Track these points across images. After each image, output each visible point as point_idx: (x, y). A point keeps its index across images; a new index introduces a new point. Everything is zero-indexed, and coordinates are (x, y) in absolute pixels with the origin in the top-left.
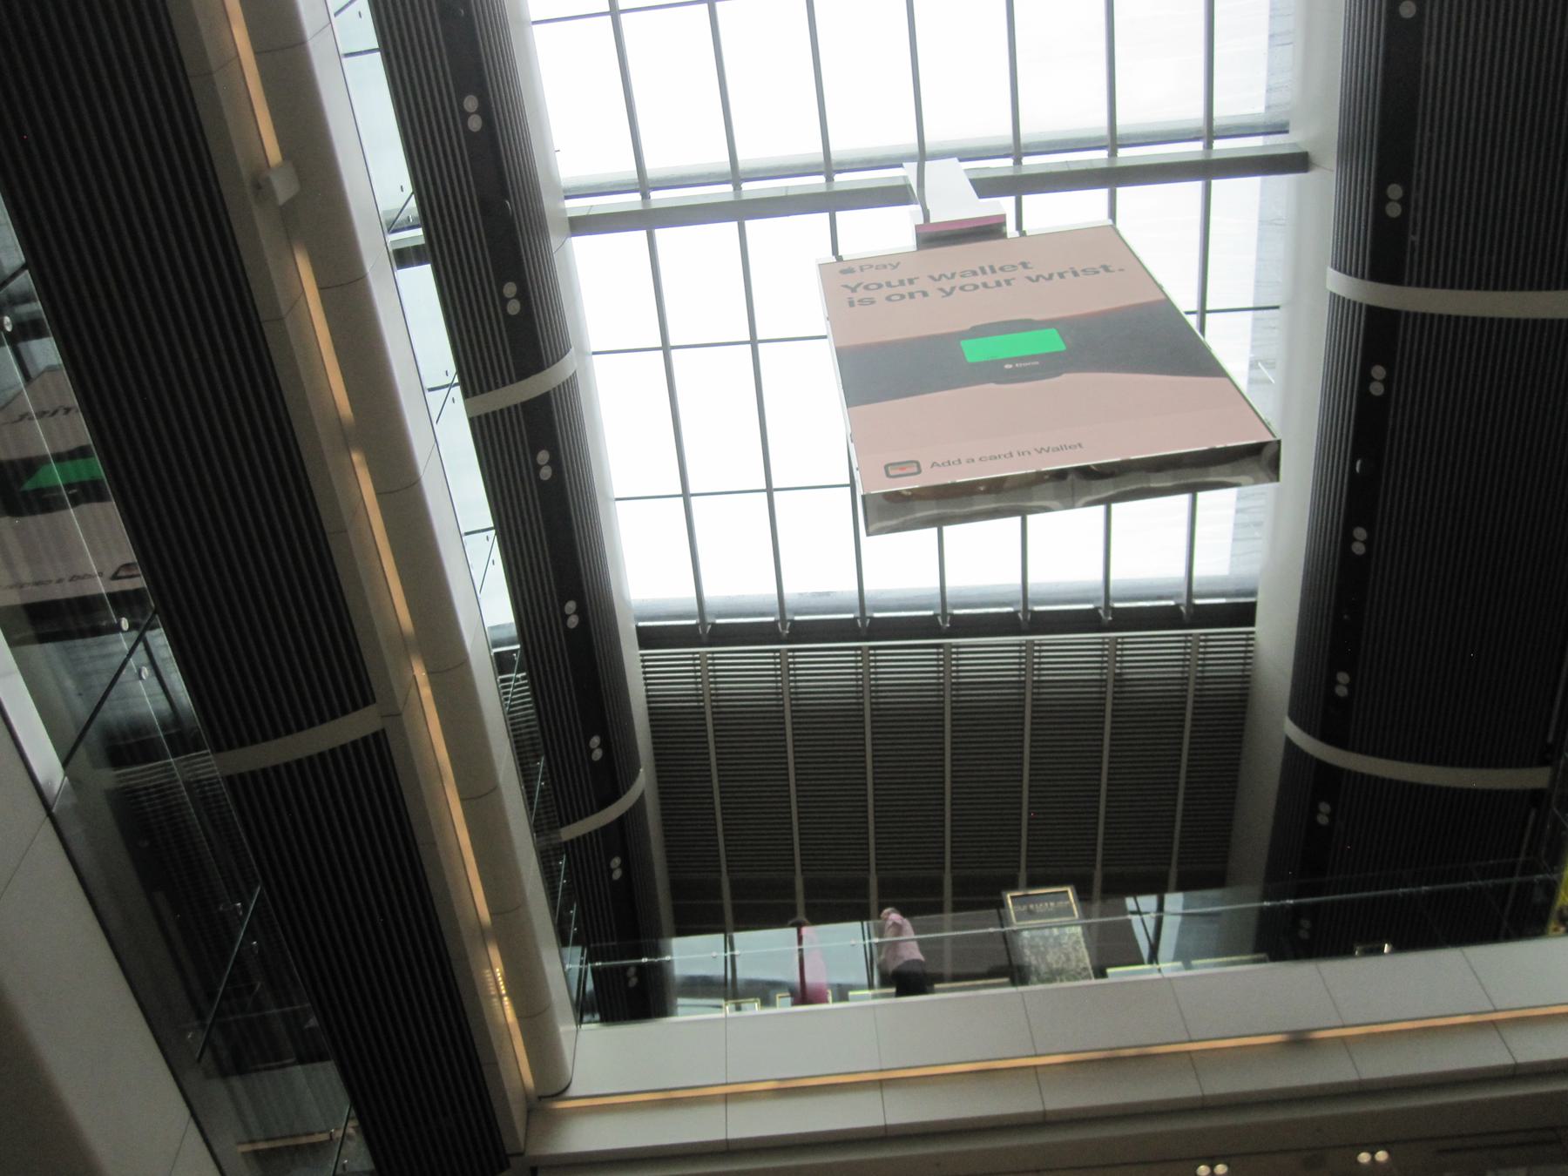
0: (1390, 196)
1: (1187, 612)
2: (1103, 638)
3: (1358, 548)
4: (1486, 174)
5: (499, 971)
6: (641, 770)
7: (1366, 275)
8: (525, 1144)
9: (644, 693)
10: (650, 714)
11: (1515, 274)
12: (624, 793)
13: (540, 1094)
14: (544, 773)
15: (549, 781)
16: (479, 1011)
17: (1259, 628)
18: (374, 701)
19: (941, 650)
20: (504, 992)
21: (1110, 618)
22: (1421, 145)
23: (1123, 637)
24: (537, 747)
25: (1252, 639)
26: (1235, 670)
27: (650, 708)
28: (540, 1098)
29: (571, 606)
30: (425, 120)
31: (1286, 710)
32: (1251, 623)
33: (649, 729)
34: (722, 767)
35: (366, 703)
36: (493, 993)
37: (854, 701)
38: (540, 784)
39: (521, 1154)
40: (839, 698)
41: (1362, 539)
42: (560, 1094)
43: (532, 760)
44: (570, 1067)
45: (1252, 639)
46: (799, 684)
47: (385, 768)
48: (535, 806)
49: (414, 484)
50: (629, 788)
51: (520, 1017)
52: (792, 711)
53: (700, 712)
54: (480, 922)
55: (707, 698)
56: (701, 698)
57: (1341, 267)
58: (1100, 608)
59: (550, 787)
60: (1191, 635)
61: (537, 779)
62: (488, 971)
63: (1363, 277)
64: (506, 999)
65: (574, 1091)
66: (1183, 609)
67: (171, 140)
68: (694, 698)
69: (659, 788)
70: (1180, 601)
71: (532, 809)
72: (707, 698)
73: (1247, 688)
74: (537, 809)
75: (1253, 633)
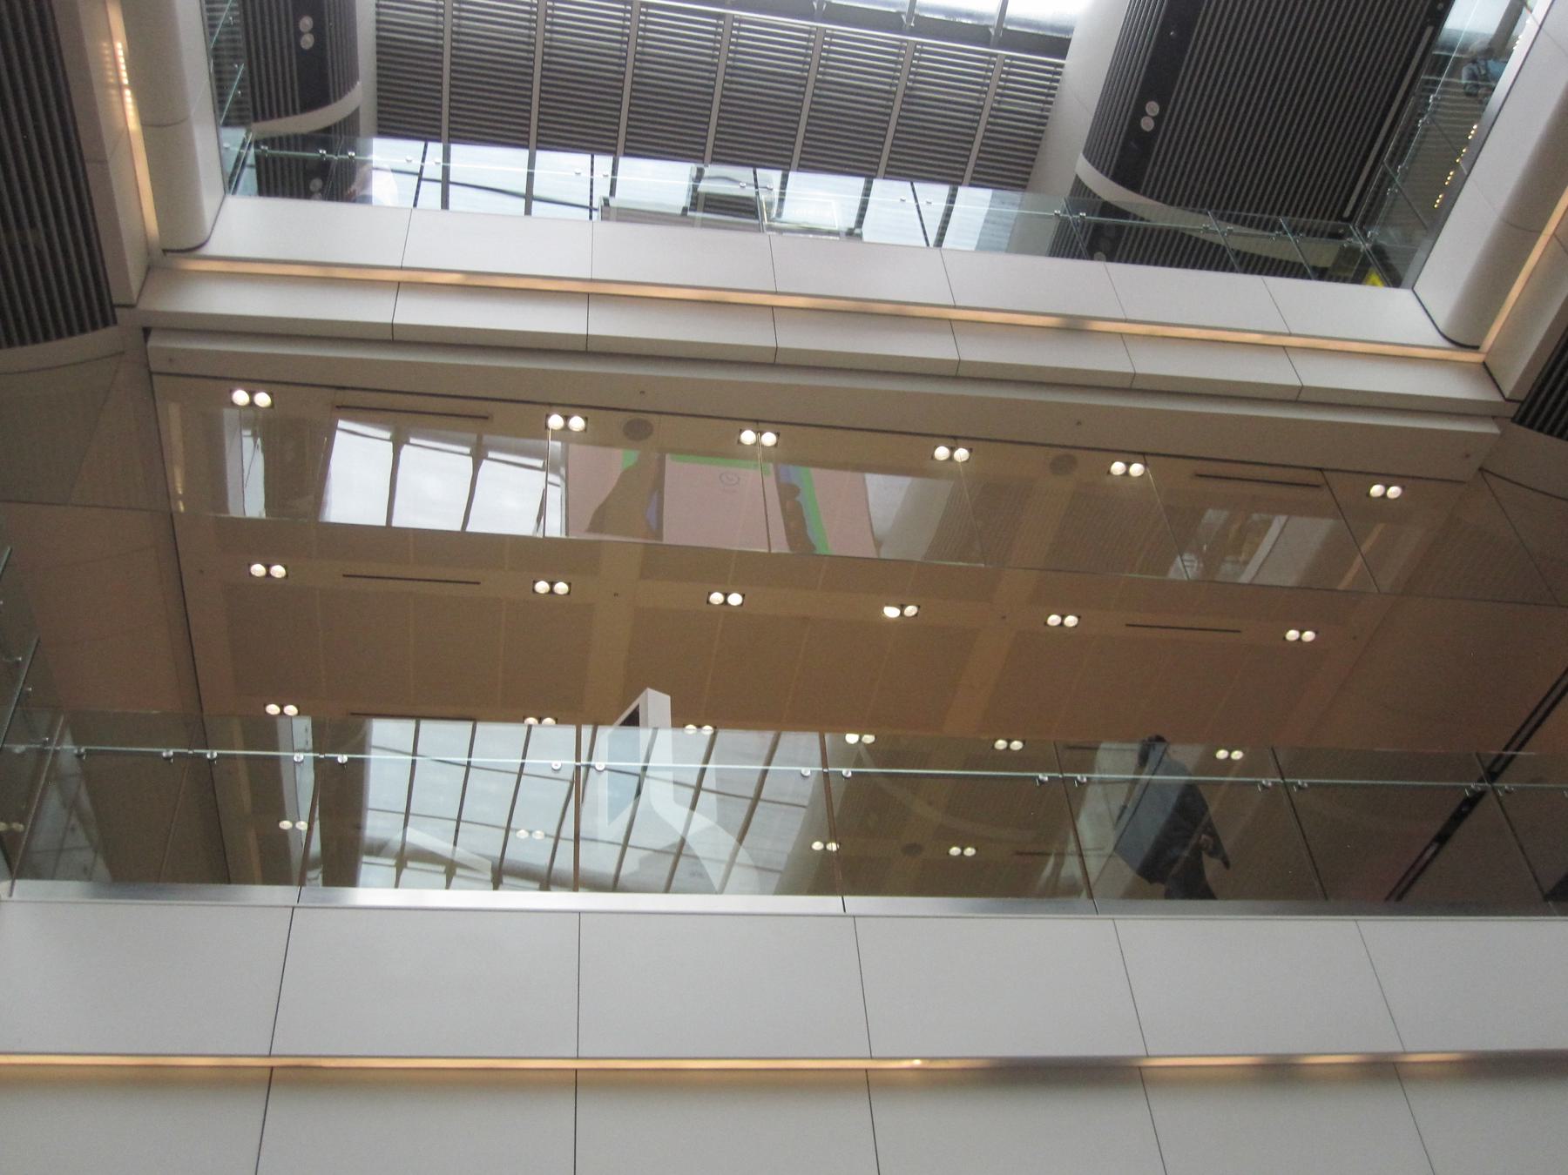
0: (1147, 110)
1: (997, 34)
2: (902, 41)
3: (1147, 124)
4: (1219, 129)
5: (120, 48)
6: (359, 83)
7: (1111, 173)
8: (140, 294)
9: (374, 17)
10: (379, 45)
11: (1283, 80)
12: (335, 100)
13: (167, 247)
14: (242, 80)
15: (249, 91)
16: (93, 116)
17: (1071, 62)
18: (115, 322)
19: (721, 22)
20: (126, 81)
21: (912, 25)
22: (1151, 174)
23: (923, 44)
24: (244, 106)
25: (1059, 73)
26: (1032, 108)
27: (378, 37)
28: (165, 251)
29: (306, 23)
30: (564, 113)
31: (1082, 147)
32: (1063, 55)
33: (375, 79)
34: (454, 126)
35: (106, 324)
36: (112, 81)
37: (615, 68)
38: (233, 91)
39: (131, 306)
40: (595, 69)
41: (1153, 115)
42: (192, 251)
43: (223, 45)
44: (208, 224)
45: (1059, 73)
46: (555, 36)
47: (63, 123)
48: (227, 106)
49: (182, 121)
50: (341, 97)
51: (145, 124)
52: (543, 69)
53: (437, 51)
54: (146, 235)
55: (447, 36)
56: (441, 11)
57: (1091, 154)
58: (903, 13)
59: (249, 99)
60: (995, 55)
61: (231, 87)
62: (105, 45)
63: (1107, 175)
64: (128, 93)
65: (212, 249)
66: (992, 31)
67: (1232, 49)
68: (431, 33)
69: (379, 97)
70: (991, 23)
71: (212, 34)
72: (447, 36)
73: (1040, 139)
74: (229, 110)
75: (1062, 66)
